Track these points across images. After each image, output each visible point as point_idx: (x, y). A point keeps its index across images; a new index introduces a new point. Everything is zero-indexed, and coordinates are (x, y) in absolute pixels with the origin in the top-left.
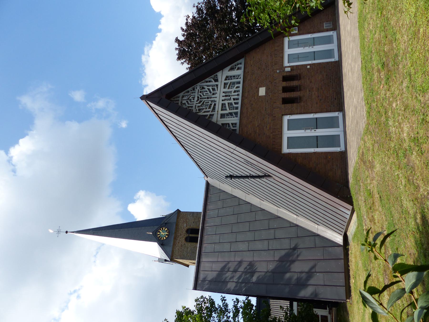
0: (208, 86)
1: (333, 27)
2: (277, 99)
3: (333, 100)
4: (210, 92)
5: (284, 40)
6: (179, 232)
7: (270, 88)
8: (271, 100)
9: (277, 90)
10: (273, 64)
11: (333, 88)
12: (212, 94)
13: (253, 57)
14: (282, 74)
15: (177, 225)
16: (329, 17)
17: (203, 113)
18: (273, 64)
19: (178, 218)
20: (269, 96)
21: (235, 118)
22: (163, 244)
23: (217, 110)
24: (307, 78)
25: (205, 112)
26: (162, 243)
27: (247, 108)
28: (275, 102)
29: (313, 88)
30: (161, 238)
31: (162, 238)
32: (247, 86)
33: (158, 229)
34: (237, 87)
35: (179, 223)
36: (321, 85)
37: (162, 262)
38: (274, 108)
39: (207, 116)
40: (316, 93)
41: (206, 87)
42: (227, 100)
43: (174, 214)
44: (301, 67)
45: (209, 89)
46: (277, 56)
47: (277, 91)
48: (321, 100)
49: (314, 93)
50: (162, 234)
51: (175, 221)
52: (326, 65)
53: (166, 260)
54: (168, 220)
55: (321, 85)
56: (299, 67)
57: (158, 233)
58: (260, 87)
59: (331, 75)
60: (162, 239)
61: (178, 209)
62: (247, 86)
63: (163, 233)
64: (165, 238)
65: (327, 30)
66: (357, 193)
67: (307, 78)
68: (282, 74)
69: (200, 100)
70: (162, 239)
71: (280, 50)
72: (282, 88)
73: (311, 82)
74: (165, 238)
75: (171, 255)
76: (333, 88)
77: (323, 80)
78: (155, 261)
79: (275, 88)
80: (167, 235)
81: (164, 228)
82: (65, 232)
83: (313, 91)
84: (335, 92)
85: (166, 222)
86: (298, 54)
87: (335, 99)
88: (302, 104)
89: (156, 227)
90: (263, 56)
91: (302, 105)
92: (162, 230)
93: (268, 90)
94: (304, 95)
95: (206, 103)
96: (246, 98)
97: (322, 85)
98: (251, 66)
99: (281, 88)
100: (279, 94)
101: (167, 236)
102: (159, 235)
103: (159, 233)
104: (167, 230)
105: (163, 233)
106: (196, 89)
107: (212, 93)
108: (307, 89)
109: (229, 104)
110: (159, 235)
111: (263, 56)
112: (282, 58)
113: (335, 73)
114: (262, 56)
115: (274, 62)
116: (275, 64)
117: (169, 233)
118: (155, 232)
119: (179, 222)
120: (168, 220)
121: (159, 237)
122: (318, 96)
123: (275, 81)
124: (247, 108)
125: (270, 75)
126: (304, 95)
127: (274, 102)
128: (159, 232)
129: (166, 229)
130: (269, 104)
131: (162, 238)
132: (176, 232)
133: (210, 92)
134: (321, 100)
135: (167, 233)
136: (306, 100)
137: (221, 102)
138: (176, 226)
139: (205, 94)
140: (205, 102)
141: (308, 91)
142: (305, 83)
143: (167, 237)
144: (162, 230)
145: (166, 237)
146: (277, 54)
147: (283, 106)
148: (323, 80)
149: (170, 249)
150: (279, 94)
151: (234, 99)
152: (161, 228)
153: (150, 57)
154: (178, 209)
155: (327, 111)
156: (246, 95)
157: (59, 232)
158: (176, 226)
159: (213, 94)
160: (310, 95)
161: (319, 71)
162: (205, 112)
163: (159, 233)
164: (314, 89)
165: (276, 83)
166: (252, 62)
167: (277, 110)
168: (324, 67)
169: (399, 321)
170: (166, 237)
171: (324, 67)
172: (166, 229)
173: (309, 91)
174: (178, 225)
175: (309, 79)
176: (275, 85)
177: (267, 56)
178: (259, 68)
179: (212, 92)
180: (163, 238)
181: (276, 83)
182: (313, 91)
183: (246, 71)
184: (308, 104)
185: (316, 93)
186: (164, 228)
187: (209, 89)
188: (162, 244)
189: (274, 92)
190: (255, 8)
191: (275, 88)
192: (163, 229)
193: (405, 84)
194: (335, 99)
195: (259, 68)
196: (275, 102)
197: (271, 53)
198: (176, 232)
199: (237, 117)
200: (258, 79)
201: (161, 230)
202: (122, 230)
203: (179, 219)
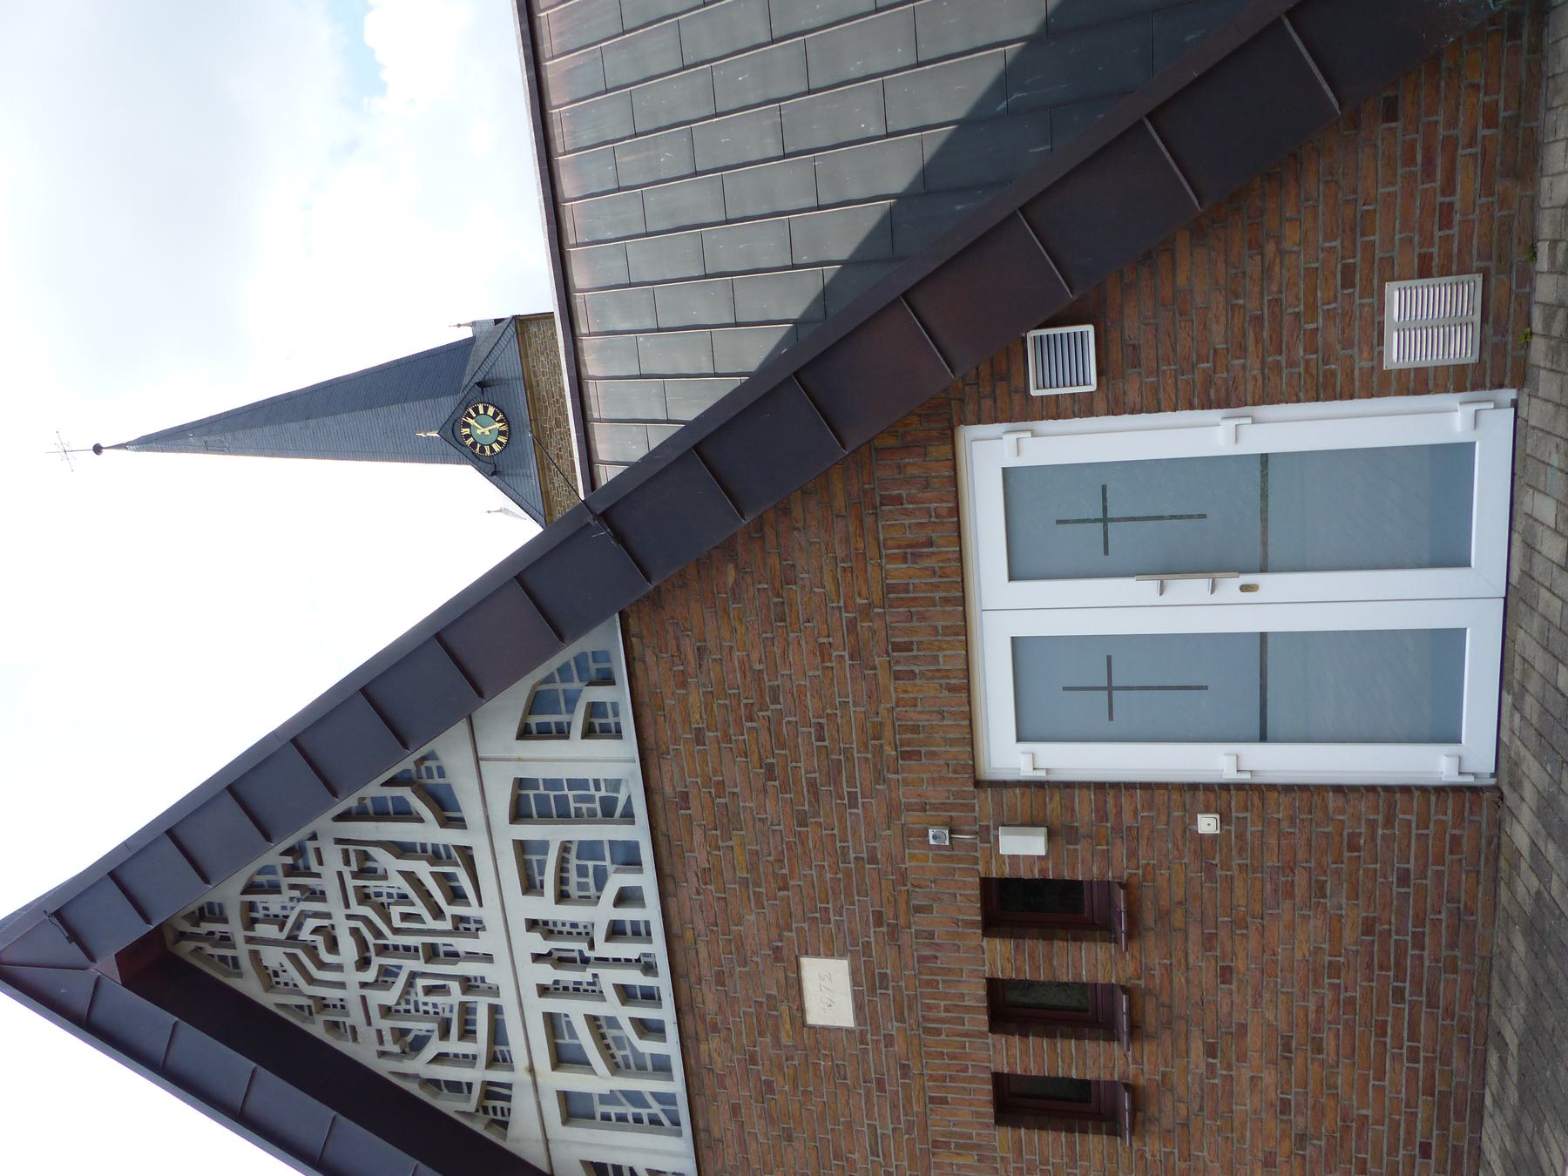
0: (402, 850)
1: (1487, 356)
2: (952, 1079)
3: (1402, 1152)
4: (438, 913)
5: (956, 434)
6: (546, 413)
7: (884, 976)
8: (904, 1076)
9: (942, 1003)
10: (890, 751)
11: (1414, 1056)
12: (447, 925)
13: (701, 651)
14: (975, 861)
15: (531, 387)
16: (1449, 187)
17: (432, 1061)
18: (890, 751)
19: (523, 356)
20: (889, 1041)
23: (526, 1063)
24: (1195, 934)
25: (440, 1058)
26: (493, 470)
27: (735, 1110)
28: (944, 1101)
29: (1243, 1027)
30: (482, 450)
31: (487, 448)
32: (700, 926)
33: (458, 415)
34: (625, 898)
35: (536, 376)
36: (1312, 1016)
38: (936, 1144)
40: (1265, 1075)
41: (383, 859)
42: (576, 990)
44: (1136, 812)
45: (409, 876)
46: (917, 669)
47: (947, 1010)
48: (1302, 1139)
49: (1247, 1074)
50: (479, 432)
51: (518, 371)
52: (1372, 824)
54: (485, 368)
55: (1312, 1016)
56: (1119, 813)
57: (464, 430)
58: (801, 955)
59: (1411, 929)
60: (488, 453)
62: (700, 926)
63: (483, 430)
64: (497, 448)
65: (1418, 382)
67: (1195, 934)
68: (975, 861)
69: (377, 961)
70: (488, 453)
71: (937, 595)
72: (982, 992)
73: (1226, 974)
74: (497, 448)
75: (542, 512)
76: (1414, 1056)
77: (1334, 970)
78: (489, 512)
79: (928, 983)
80: (501, 433)
81: (481, 408)
82: (92, 448)
83: (1242, 1057)
84: (1432, 1095)
85: (479, 378)
86: (1109, 650)
87: (1425, 1151)
88: (1153, 1147)
89: (448, 404)
90: (784, 653)
91: (1148, 1156)
92: (474, 415)
93: (872, 990)
94: (1164, 1074)
95: (429, 990)
96: (715, 1028)
97: (1319, 1009)
98: (700, 740)
99: (975, 993)
100: (967, 1035)
101: (503, 439)
103: (466, 431)
104: (495, 415)
106: (321, 863)
108: (1196, 1032)
109: (613, 730)
111: (784, 653)
112: (963, 685)
113: (1443, 916)
114: (777, 651)
115: (888, 732)
116: (906, 756)
117: (506, 421)
119: (534, 372)
120: (485, 368)
121: (474, 445)
122: (1285, 1106)
123: (921, 922)
124: (735, 1110)
125: (873, 859)
126: (1164, 1074)
127: (932, 1100)
128: (467, 425)
129: (491, 411)
130: (894, 1106)
131: (487, 448)
132: (535, 414)
133: (438, 913)
134: (1302, 1139)
135: (498, 425)
136: (1185, 1125)
137: (538, 1007)
138: (528, 391)
139: (397, 923)
140: (421, 983)
141: (1197, 1046)
142: (1179, 978)
143: (504, 441)
144: (474, 415)
145: (500, 443)
146: (907, 647)
147: (1004, 1137)
148: (1334, 970)
149: (531, 485)
150: (967, 1035)
151: (626, 994)
152: (466, 409)
156: (708, 998)
158: (528, 391)
159: (462, 926)
160: (1216, 1081)
161: (1300, 879)
162: (440, 1058)
163: (466, 431)
164: (1252, 1040)
165: (931, 935)
166: (695, 698)
167: (960, 1161)
168: (1353, 837)
170: (500, 443)
171: (1353, 837)
172: (491, 411)
173: (1211, 1051)
174: (535, 384)
175: (1209, 942)
176: (927, 952)
177: (824, 652)
178: (770, 768)
179: (450, 910)
180: (492, 450)
181: (931, 935)
182: (1242, 1057)
183: (668, 790)
184: (1198, 1158)
185: (1269, 1077)
186: (481, 408)
187: (409, 876)
188: (494, 470)
189: (926, 1019)
191: (928, 983)
192: (476, 410)
194: (1425, 1151)
195: (770, 772)
196: (944, 1101)
197: (852, 626)
198: (535, 414)
200: (775, 875)
201: (472, 418)
202: (312, 423)
203: (530, 359)
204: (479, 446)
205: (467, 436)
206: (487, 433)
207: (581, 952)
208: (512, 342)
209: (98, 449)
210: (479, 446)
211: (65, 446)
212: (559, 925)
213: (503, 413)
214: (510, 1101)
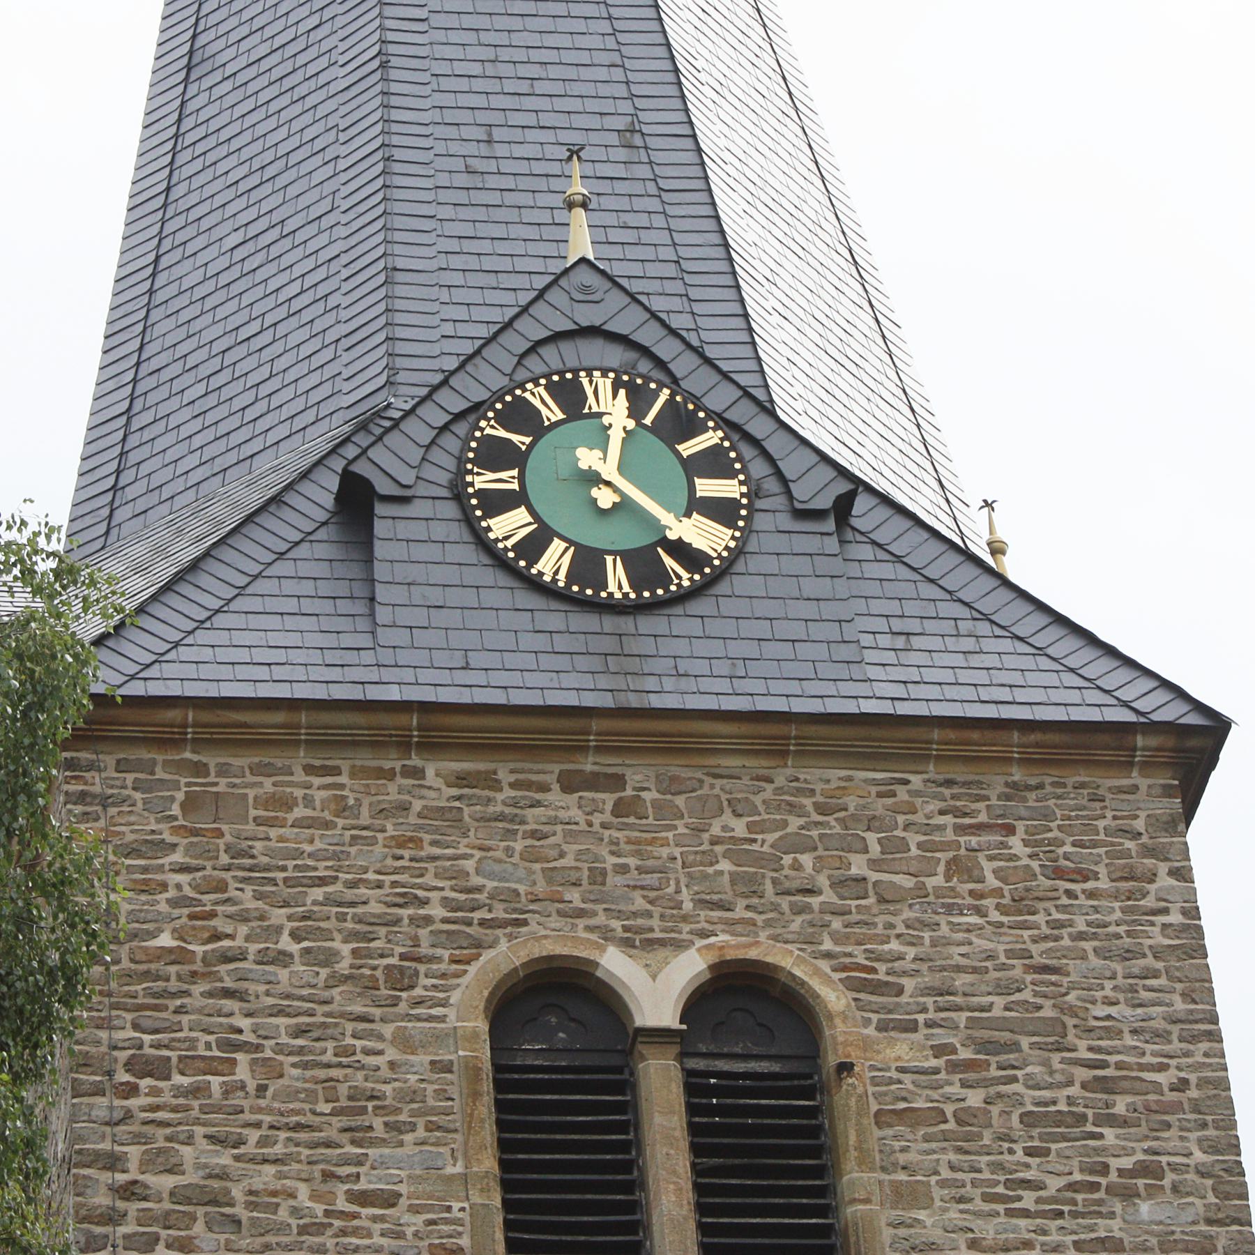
26: (383, 486)
31: (507, 479)
39: (1001, 869)
43: (1099, 667)
50: (587, 458)
60: (483, 480)
66: (685, 1218)
70: (483, 480)
102: (552, 413)
105: (609, 471)
107: (251, 820)
110: (552, 413)
118: (587, 316)
121: (521, 417)
131: (507, 479)
145: (534, 546)
155: (794, 1138)
169: (661, 3)
170: (534, 546)
180: (498, 503)
201: (636, 412)
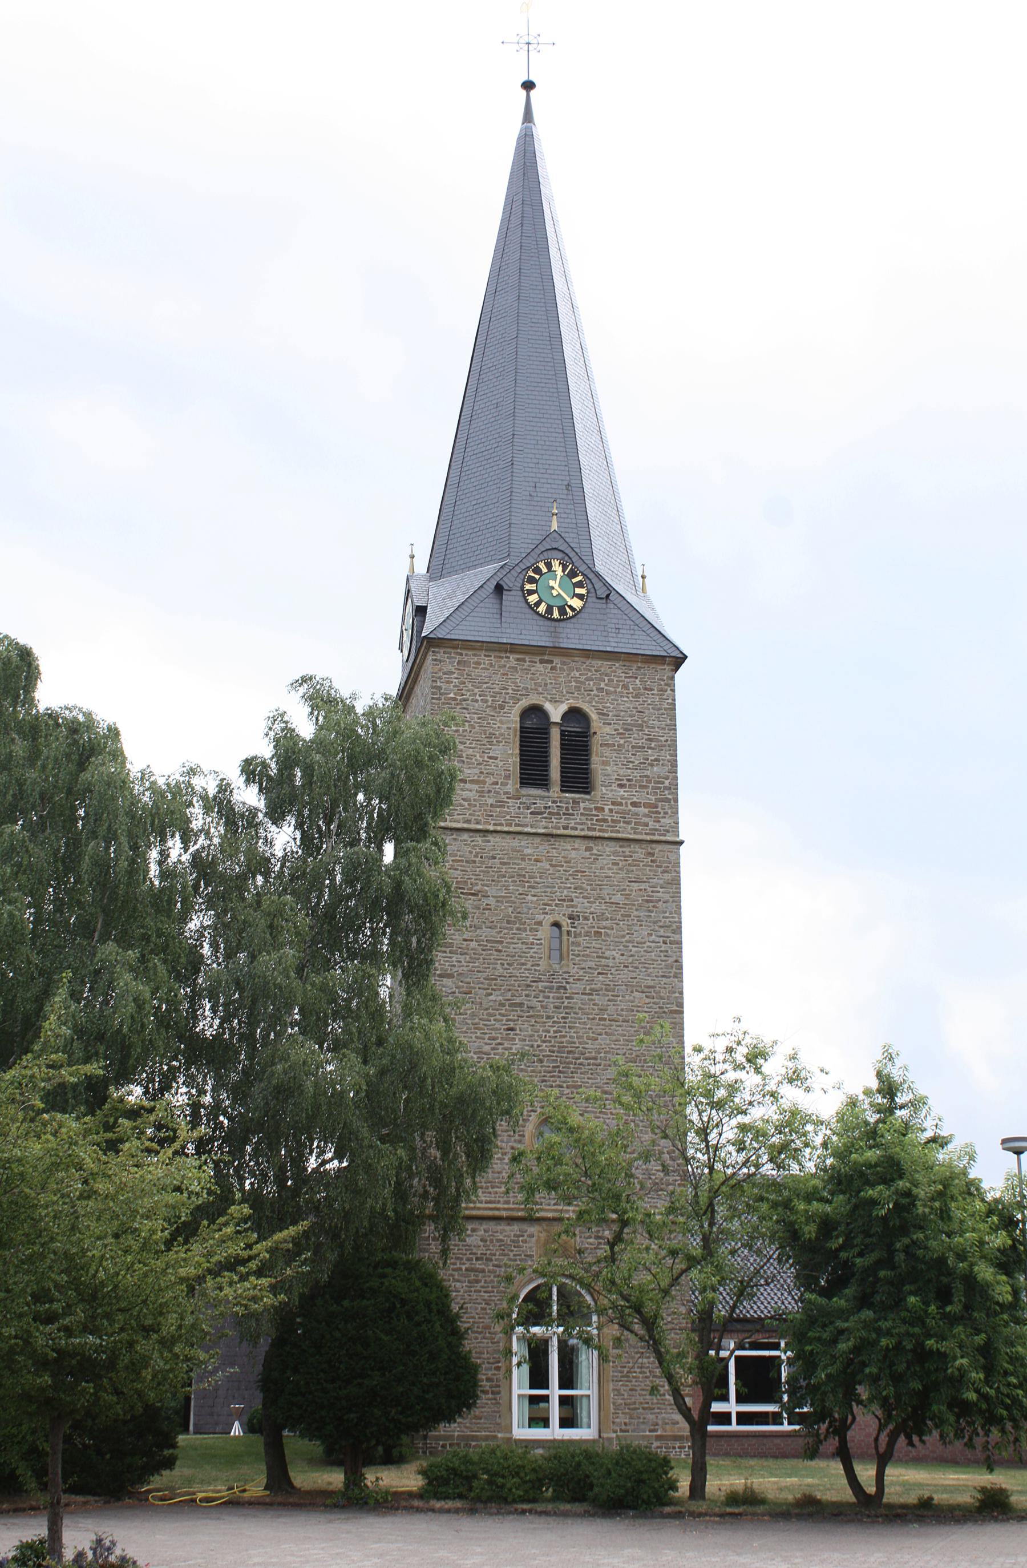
21: (588, 1430)
22: (505, 592)
30: (531, 580)
31: (533, 587)
37: (408, 592)
50: (552, 583)
53: (421, 611)
60: (528, 587)
61: (685, 657)
63: (556, 586)
64: (533, 599)
70: (528, 587)
74: (533, 599)
78: (412, 557)
81: (582, 591)
82: (531, 78)
102: (544, 570)
105: (556, 586)
110: (544, 570)
121: (537, 570)
131: (533, 587)
145: (538, 604)
153: (930, 1102)
154: (685, 657)
157: (528, 44)
170: (538, 604)
180: (531, 592)
186: (582, 591)
190: (847, 1320)
193: (608, 1107)
199: (589, 1427)
204: (537, 577)
205: (580, 585)
206: (555, 593)
207: (436, 1158)
208: (659, 648)
209: (528, 86)
210: (537, 577)
211: (535, 46)
212: (774, 1067)
213: (573, 617)
214: (548, 1402)
